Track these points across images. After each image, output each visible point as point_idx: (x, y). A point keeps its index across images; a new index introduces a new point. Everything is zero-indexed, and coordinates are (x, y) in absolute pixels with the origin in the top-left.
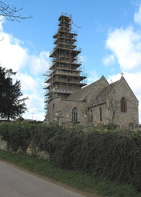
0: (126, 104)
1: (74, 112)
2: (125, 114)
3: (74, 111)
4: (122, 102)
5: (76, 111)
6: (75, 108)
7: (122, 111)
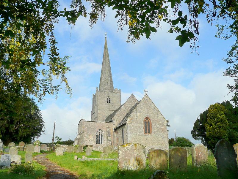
0: (151, 125)
1: (98, 135)
2: (149, 136)
3: (98, 133)
4: (145, 122)
5: (101, 133)
6: (99, 130)
7: (146, 132)
